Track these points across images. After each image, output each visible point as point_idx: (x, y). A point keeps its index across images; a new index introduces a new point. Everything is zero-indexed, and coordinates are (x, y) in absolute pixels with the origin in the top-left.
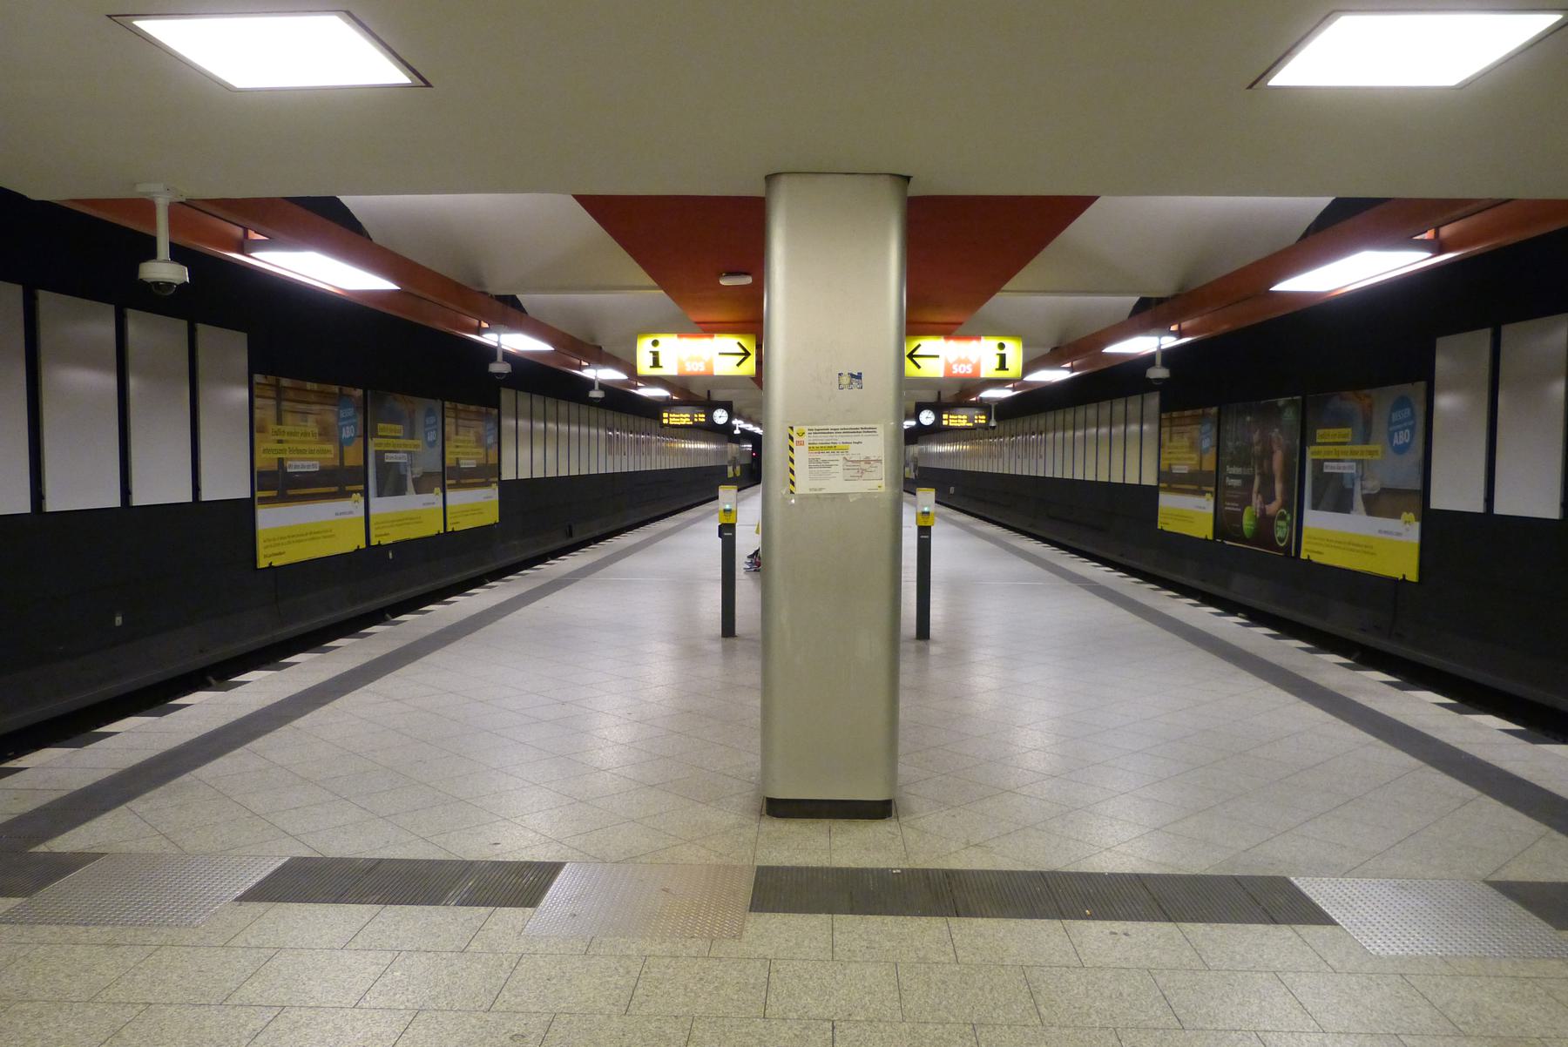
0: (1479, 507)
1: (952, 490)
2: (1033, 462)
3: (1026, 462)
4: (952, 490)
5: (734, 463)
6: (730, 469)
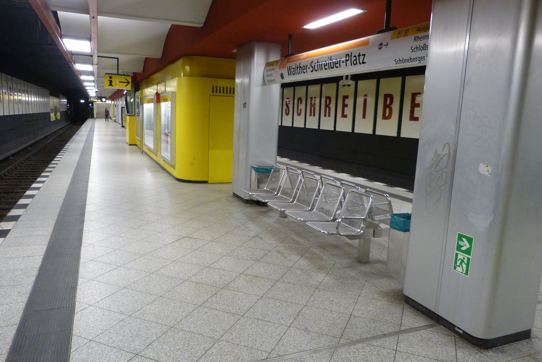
5: (55, 110)
6: (52, 115)
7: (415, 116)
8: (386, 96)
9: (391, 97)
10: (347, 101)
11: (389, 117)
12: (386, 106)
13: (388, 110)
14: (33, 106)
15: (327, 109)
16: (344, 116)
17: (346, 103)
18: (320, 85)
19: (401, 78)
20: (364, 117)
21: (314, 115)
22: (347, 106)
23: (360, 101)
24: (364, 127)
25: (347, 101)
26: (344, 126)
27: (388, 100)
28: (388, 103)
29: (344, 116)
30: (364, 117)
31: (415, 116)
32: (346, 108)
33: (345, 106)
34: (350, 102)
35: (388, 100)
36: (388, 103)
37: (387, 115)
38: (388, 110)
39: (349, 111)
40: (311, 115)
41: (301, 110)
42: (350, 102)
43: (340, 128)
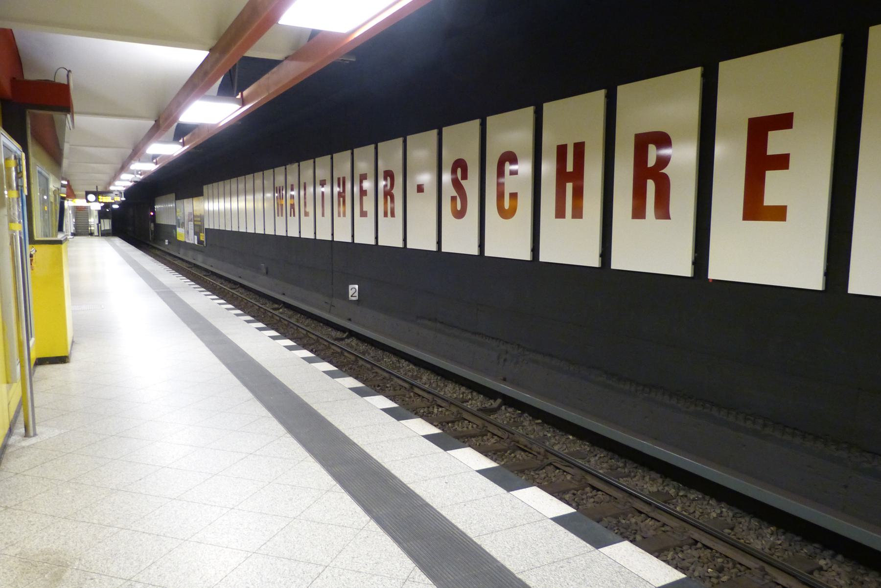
0: (527, 256)
1: (353, 290)
3: (281, 221)
4: (353, 290)
15: (651, 185)
16: (363, 214)
20: (323, 215)
22: (782, 162)
29: (363, 214)
30: (323, 215)
33: (760, 163)
40: (339, 216)
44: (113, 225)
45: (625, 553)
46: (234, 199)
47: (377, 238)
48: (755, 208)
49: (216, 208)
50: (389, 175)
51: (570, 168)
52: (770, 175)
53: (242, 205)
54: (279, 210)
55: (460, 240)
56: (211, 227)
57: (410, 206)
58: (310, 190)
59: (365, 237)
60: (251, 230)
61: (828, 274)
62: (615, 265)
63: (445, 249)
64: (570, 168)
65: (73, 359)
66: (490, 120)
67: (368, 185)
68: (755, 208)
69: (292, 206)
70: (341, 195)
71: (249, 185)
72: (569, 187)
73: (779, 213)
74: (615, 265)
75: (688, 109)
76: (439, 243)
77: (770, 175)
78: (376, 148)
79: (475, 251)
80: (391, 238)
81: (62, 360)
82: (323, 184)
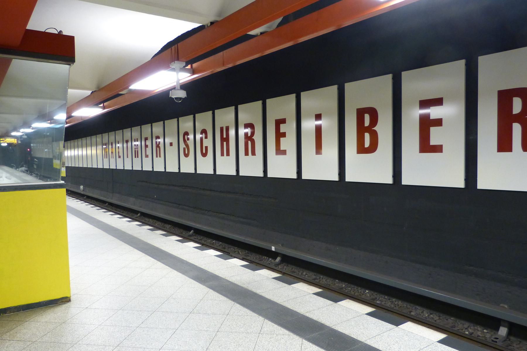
2: (113, 161)
7: (433, 142)
8: (361, 113)
9: (374, 114)
10: (283, 128)
11: (373, 148)
12: (361, 130)
13: (367, 136)
14: (121, 154)
15: (250, 142)
16: (147, 156)
17: (282, 131)
18: (260, 103)
19: (294, 95)
20: (127, 157)
21: (228, 154)
22: (284, 135)
23: (309, 125)
24: (321, 167)
25: (283, 128)
26: (282, 168)
27: (367, 117)
28: (367, 123)
29: (147, 156)
30: (127, 157)
31: (433, 142)
32: (282, 139)
33: (280, 135)
34: (289, 128)
35: (367, 117)
36: (367, 123)
37: (367, 144)
38: (367, 136)
39: (289, 143)
40: (247, 154)
41: (206, 148)
42: (289, 128)
43: (185, 169)
44: (52, 165)
45: (409, 326)
46: (84, 149)
47: (165, 168)
48: (426, 147)
49: (69, 155)
50: (204, 132)
51: (225, 136)
52: (282, 139)
53: (84, 153)
54: (106, 155)
55: (187, 168)
56: (70, 165)
57: (168, 153)
58: (114, 145)
59: (147, 167)
60: (81, 166)
61: (467, 180)
62: (304, 177)
63: (271, 174)
64: (225, 136)
65: (74, 293)
66: (197, 115)
67: (149, 143)
68: (426, 147)
69: (112, 152)
70: (249, 138)
71: (80, 143)
72: (225, 143)
73: (438, 149)
74: (304, 177)
75: (191, 124)
76: (179, 168)
77: (282, 139)
78: (164, 123)
79: (212, 172)
80: (159, 168)
81: (66, 300)
82: (158, 137)
